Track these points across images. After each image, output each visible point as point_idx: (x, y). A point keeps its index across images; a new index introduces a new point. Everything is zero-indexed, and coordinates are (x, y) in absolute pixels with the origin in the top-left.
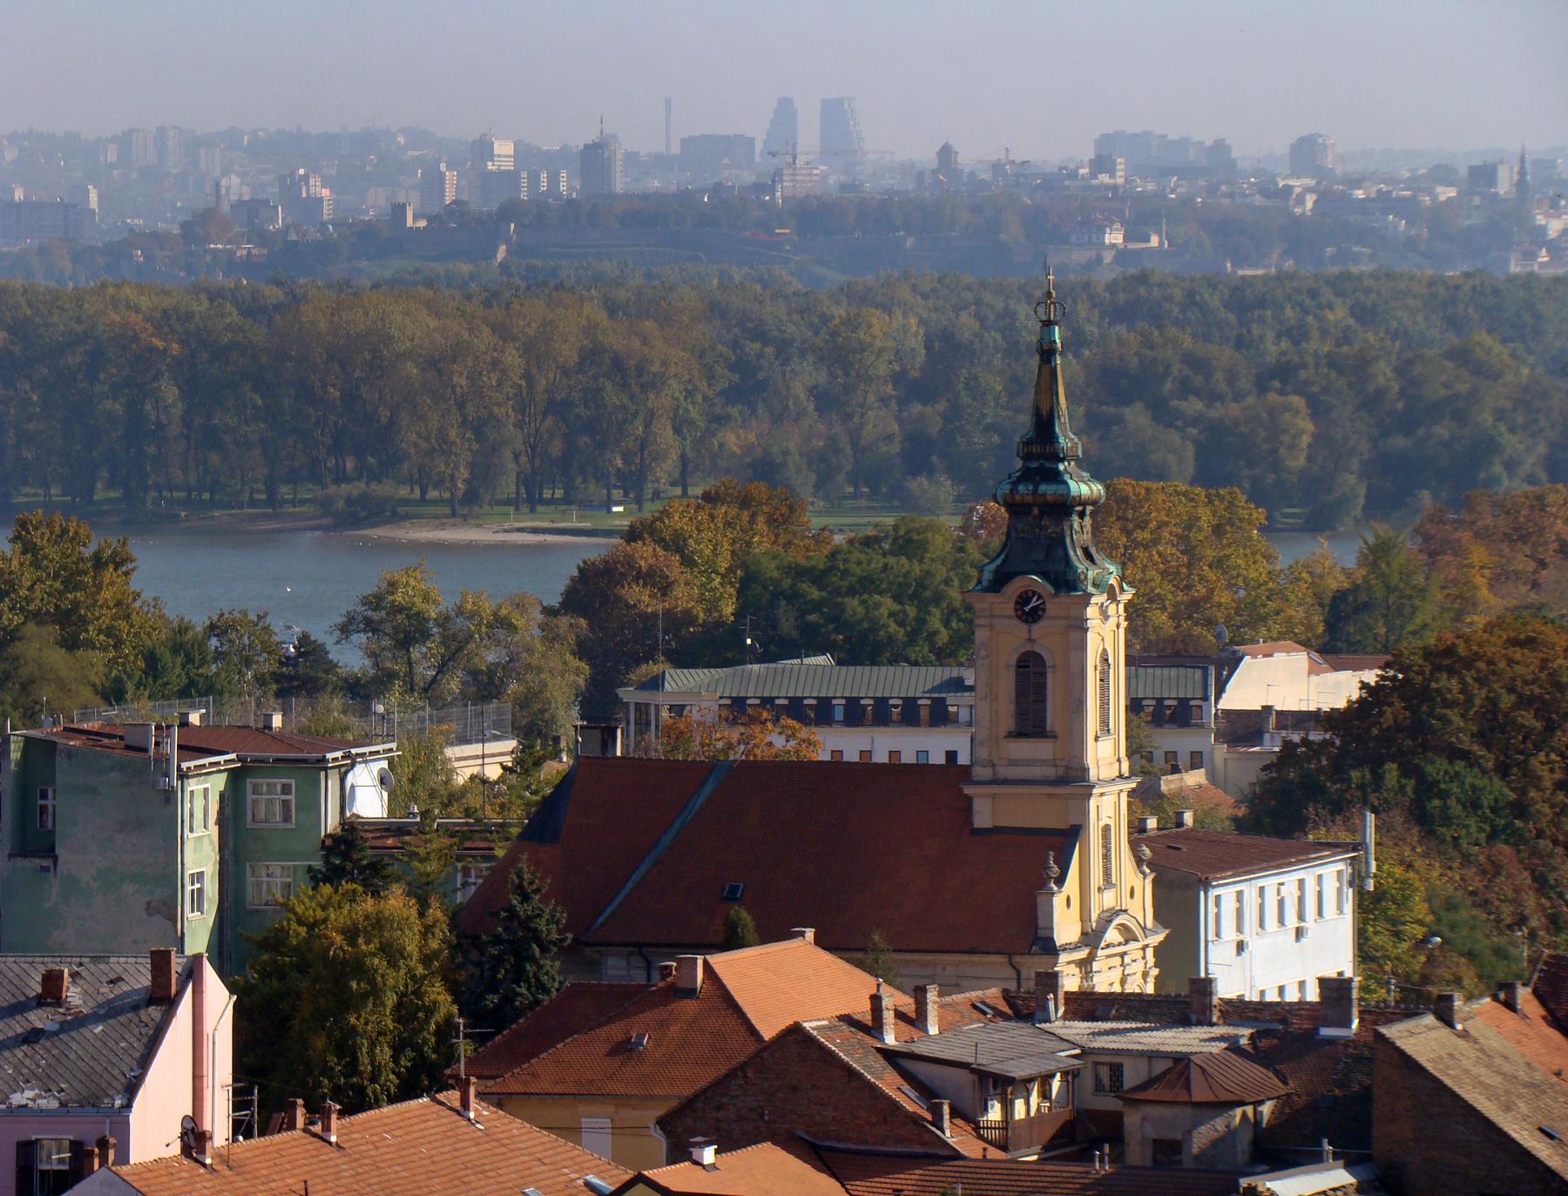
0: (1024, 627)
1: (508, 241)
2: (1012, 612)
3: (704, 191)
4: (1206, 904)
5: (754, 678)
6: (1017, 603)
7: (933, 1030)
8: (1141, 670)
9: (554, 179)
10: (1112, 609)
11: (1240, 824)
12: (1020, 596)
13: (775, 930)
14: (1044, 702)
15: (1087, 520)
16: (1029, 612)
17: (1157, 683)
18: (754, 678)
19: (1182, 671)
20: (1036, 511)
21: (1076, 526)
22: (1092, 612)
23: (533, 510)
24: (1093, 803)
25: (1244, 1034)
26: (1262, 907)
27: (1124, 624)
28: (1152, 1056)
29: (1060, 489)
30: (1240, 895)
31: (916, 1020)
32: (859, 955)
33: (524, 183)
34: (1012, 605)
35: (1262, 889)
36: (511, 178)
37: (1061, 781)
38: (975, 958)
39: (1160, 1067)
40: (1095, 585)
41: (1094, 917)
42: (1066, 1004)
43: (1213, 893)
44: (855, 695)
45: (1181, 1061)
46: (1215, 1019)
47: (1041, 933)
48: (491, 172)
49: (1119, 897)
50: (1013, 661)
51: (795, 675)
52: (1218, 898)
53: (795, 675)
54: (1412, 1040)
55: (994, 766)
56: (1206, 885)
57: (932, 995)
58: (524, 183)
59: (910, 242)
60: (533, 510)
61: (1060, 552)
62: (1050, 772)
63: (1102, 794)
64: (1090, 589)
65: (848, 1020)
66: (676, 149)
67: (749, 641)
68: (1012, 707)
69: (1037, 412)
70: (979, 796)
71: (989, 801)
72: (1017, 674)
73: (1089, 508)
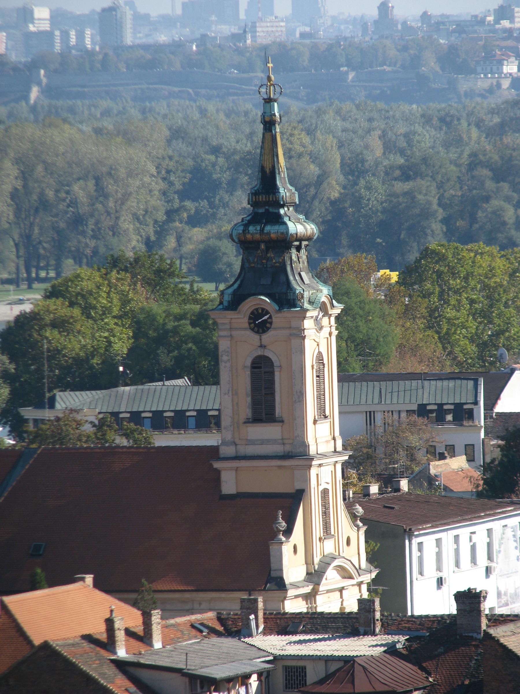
0: (256, 337)
1: (39, 84)
2: (246, 325)
3: (192, 42)
4: (412, 548)
5: (125, 397)
6: (250, 318)
7: (158, 645)
8: (426, 383)
9: (81, 36)
10: (325, 321)
11: (480, 495)
12: (252, 313)
13: (63, 576)
14: (273, 394)
15: (303, 253)
16: (260, 323)
17: (439, 392)
18: (125, 397)
19: (458, 382)
20: (263, 246)
21: (294, 258)
22: (308, 324)
23: (30, 287)
24: (313, 472)
25: (400, 640)
26: (457, 552)
27: (335, 333)
28: (328, 659)
29: (281, 228)
30: (438, 542)
31: (145, 638)
32: (133, 596)
33: (58, 40)
34: (246, 320)
35: (457, 537)
36: (48, 35)
37: (287, 456)
38: (223, 595)
39: (334, 667)
40: (311, 302)
41: (316, 560)
42: (265, 622)
43: (415, 541)
44: (204, 408)
45: (349, 662)
46: (377, 630)
47: (273, 574)
48: (32, 33)
49: (337, 546)
50: (249, 363)
51: (157, 394)
52: (420, 544)
53: (157, 394)
54: (513, 638)
55: (236, 445)
56: (410, 534)
57: (156, 617)
58: (58, 40)
59: (351, 76)
60: (30, 287)
61: (283, 278)
62: (278, 449)
63: (320, 465)
64: (306, 305)
65: (88, 638)
66: (179, 11)
67: (121, 369)
68: (249, 399)
69: (262, 169)
70: (225, 469)
71: (234, 473)
72: (252, 373)
73: (304, 243)
